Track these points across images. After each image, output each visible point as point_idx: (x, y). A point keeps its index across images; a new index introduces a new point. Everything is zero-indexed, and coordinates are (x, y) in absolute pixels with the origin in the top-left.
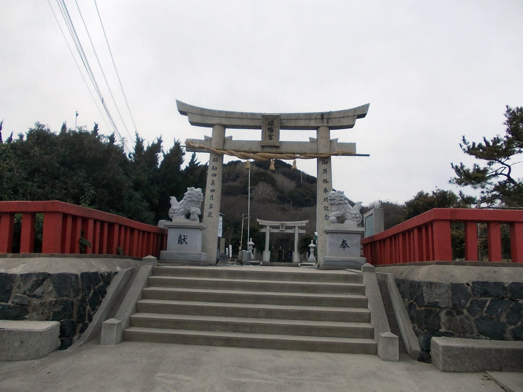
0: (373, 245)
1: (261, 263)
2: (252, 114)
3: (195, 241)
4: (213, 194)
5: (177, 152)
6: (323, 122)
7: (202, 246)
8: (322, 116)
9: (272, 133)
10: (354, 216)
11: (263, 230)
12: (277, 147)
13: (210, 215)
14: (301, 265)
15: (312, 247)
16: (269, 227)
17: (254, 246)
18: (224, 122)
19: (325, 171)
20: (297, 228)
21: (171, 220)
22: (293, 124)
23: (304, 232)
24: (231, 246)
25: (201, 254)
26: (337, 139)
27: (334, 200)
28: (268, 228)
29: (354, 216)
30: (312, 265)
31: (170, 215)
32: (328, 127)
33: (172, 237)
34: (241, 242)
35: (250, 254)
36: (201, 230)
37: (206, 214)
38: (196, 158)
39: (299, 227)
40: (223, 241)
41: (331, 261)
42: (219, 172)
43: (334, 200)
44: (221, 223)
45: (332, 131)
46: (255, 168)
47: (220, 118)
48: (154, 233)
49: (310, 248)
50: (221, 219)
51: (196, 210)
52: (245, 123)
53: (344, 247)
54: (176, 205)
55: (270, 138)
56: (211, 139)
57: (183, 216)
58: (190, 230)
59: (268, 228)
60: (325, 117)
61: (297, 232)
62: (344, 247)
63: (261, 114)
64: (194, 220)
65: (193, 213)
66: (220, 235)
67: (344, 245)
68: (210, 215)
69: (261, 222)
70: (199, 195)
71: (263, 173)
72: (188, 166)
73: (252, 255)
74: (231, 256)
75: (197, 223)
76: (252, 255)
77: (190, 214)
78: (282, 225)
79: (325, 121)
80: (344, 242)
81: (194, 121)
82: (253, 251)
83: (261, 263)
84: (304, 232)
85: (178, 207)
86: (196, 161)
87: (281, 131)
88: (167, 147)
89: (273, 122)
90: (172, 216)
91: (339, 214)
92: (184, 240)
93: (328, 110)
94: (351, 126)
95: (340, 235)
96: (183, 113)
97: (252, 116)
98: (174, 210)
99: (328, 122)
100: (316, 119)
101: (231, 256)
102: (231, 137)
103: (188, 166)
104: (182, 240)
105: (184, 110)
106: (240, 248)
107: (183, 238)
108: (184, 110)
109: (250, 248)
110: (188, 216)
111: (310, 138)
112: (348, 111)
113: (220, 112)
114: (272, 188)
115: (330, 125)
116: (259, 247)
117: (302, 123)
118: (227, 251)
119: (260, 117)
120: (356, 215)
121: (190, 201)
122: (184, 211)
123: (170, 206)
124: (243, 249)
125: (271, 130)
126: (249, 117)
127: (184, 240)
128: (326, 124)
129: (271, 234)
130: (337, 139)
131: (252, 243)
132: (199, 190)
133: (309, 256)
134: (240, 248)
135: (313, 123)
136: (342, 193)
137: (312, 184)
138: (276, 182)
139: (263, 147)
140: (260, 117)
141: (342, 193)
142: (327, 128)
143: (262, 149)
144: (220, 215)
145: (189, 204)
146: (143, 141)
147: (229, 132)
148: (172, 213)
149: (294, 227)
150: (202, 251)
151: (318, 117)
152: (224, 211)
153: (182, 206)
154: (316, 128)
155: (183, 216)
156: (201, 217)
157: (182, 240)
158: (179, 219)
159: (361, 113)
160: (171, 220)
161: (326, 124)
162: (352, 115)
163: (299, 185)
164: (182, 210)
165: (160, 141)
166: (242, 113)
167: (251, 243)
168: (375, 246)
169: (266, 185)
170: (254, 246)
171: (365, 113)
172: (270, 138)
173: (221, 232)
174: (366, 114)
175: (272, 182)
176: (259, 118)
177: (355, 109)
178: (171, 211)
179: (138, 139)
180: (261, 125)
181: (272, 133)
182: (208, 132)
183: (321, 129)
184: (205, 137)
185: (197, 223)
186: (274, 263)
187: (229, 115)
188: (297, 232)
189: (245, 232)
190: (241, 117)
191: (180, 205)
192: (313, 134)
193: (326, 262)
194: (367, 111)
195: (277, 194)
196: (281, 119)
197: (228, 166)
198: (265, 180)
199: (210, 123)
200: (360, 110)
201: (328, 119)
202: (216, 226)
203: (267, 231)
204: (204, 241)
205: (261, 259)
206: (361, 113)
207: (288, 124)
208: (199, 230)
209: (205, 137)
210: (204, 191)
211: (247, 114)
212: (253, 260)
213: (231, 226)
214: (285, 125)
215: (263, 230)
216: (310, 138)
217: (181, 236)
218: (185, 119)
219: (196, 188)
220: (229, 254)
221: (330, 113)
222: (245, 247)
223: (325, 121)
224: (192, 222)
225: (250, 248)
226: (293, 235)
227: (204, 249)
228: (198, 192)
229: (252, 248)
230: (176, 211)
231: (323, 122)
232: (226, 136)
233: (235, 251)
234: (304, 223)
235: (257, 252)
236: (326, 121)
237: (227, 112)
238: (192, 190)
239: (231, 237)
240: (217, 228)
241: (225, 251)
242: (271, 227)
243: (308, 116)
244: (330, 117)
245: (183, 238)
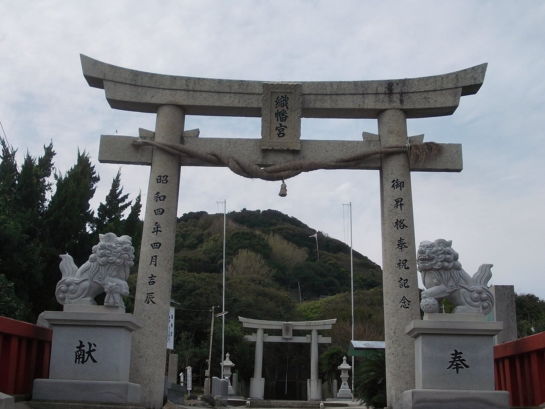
0: (501, 365)
1: (248, 402)
2: (241, 83)
3: (115, 354)
4: (156, 252)
5: (82, 177)
6: (391, 101)
7: (131, 369)
8: (390, 88)
9: (283, 124)
10: (476, 295)
11: (250, 338)
12: (295, 152)
13: (150, 299)
14: (326, 405)
15: (345, 370)
16: (260, 332)
17: (233, 369)
18: (182, 99)
19: (399, 203)
20: (314, 334)
21: (60, 308)
22: (328, 104)
23: (327, 340)
24: (189, 369)
25: (127, 386)
26: (423, 135)
27: (432, 259)
28: (260, 333)
29: (476, 295)
30: (346, 405)
31: (59, 296)
32: (401, 109)
33: (63, 346)
34: (209, 361)
35: (225, 384)
36: (131, 330)
37: (140, 296)
38: (120, 188)
39: (320, 332)
40: (174, 358)
41: (431, 401)
42: (168, 238)
43: (432, 259)
44: (172, 321)
45: (410, 122)
46: (234, 226)
47: (173, 92)
48: (20, 339)
49: (340, 372)
50: (172, 311)
51: (117, 284)
52: (227, 101)
53: (457, 367)
54: (74, 273)
55: (281, 134)
56: (153, 135)
57: (89, 299)
58: (103, 330)
59: (260, 333)
60: (396, 90)
61: (315, 341)
62: (457, 367)
63: (259, 82)
64: (114, 307)
65: (112, 291)
66: (170, 345)
67: (457, 362)
68: (150, 299)
69: (247, 322)
70: (126, 250)
71: (247, 234)
72: (105, 203)
73: (230, 386)
74: (189, 388)
75: (120, 314)
76: (230, 386)
77: (104, 294)
78: (287, 328)
79: (396, 98)
80: (457, 355)
81: (119, 97)
82: (231, 379)
83: (248, 402)
84: (327, 340)
85: (76, 279)
86: (120, 192)
87: (303, 120)
88: (63, 165)
89: (286, 99)
90: (64, 299)
91: (443, 292)
92: (89, 353)
93: (403, 78)
94: (449, 111)
95: (447, 340)
96: (95, 82)
97: (242, 88)
98: (68, 285)
99: (402, 101)
100: (377, 94)
101: (189, 388)
102: (197, 132)
103: (105, 203)
104: (84, 354)
105: (98, 75)
106: (207, 373)
107: (86, 348)
108: (98, 75)
109: (226, 374)
110: (99, 298)
111: (365, 134)
112: (442, 78)
113: (174, 78)
114: (263, 261)
115: (407, 106)
116: (244, 372)
117: (348, 103)
118: (182, 379)
119: (260, 90)
120: (480, 293)
121: (104, 264)
122: (90, 287)
123: (59, 275)
124: (212, 374)
125: (282, 116)
126: (235, 88)
127: (89, 353)
128: (397, 104)
129: (267, 346)
130: (423, 135)
131: (231, 363)
132: (125, 238)
133: (339, 388)
134: (207, 373)
135: (370, 103)
136: (449, 244)
137: (335, 253)
138: (271, 250)
139: (265, 152)
140: (260, 90)
141: (449, 244)
142: (400, 113)
143: (264, 157)
144: (172, 304)
145: (102, 270)
146: (14, 154)
147: (192, 122)
148: (64, 292)
149: (309, 332)
150: (131, 380)
151: (382, 89)
152: (178, 292)
153: (86, 276)
154: (376, 114)
155: (89, 299)
156: (129, 304)
157: (84, 354)
158: (78, 306)
159: (469, 82)
160: (60, 308)
161: (397, 104)
162: (451, 86)
163: (312, 256)
164: (87, 283)
165: (49, 153)
166: (220, 81)
167: (228, 362)
168: (522, 367)
169: (252, 254)
170: (233, 369)
171: (478, 83)
172: (281, 134)
173: (172, 338)
174: (481, 85)
175: (265, 252)
176: (257, 91)
177: (457, 75)
178: (60, 286)
179: (5, 151)
180: (261, 105)
181: (283, 124)
182: (148, 121)
183: (387, 117)
184: (141, 130)
185: (120, 314)
186: (273, 402)
187: (191, 85)
188: (315, 341)
189: (217, 341)
190: (217, 89)
191: (82, 273)
192: (371, 126)
193: (418, 402)
194: (483, 79)
195: (274, 272)
196: (303, 95)
197: (182, 222)
198: (252, 247)
199: (154, 101)
200: (469, 76)
201: (402, 94)
202: (160, 323)
203: (258, 340)
204: (136, 354)
205: (247, 395)
206: (469, 82)
207: (318, 105)
208: (123, 331)
209: (141, 130)
210: (137, 243)
211: (230, 83)
212: (231, 395)
213: (191, 327)
214: (311, 106)
215: (250, 338)
216: (365, 134)
217: (82, 345)
218: (99, 94)
219: (119, 236)
220: (186, 385)
221: (404, 82)
222: (217, 371)
223: (396, 98)
224: (108, 312)
225: (226, 374)
226: (308, 346)
227: (135, 374)
228: (122, 244)
229: (229, 372)
230: (72, 287)
231: (391, 101)
232: (186, 129)
233: (198, 381)
234: (328, 323)
235: (239, 380)
236: (398, 99)
237: (188, 79)
238: (109, 239)
239: (188, 354)
240: (166, 328)
241: (179, 377)
242: (265, 331)
243: (361, 88)
244: (406, 89)
245: (86, 348)
